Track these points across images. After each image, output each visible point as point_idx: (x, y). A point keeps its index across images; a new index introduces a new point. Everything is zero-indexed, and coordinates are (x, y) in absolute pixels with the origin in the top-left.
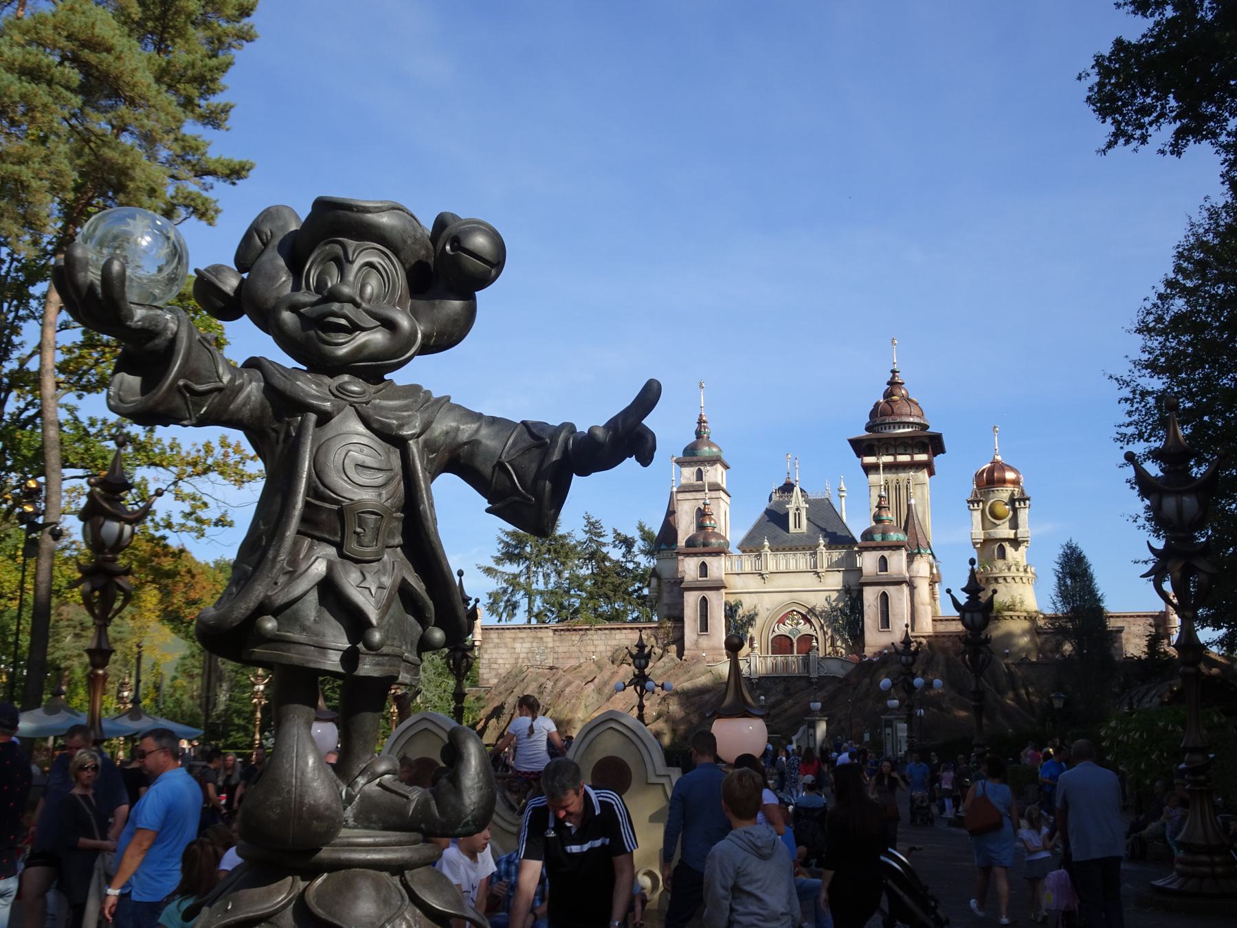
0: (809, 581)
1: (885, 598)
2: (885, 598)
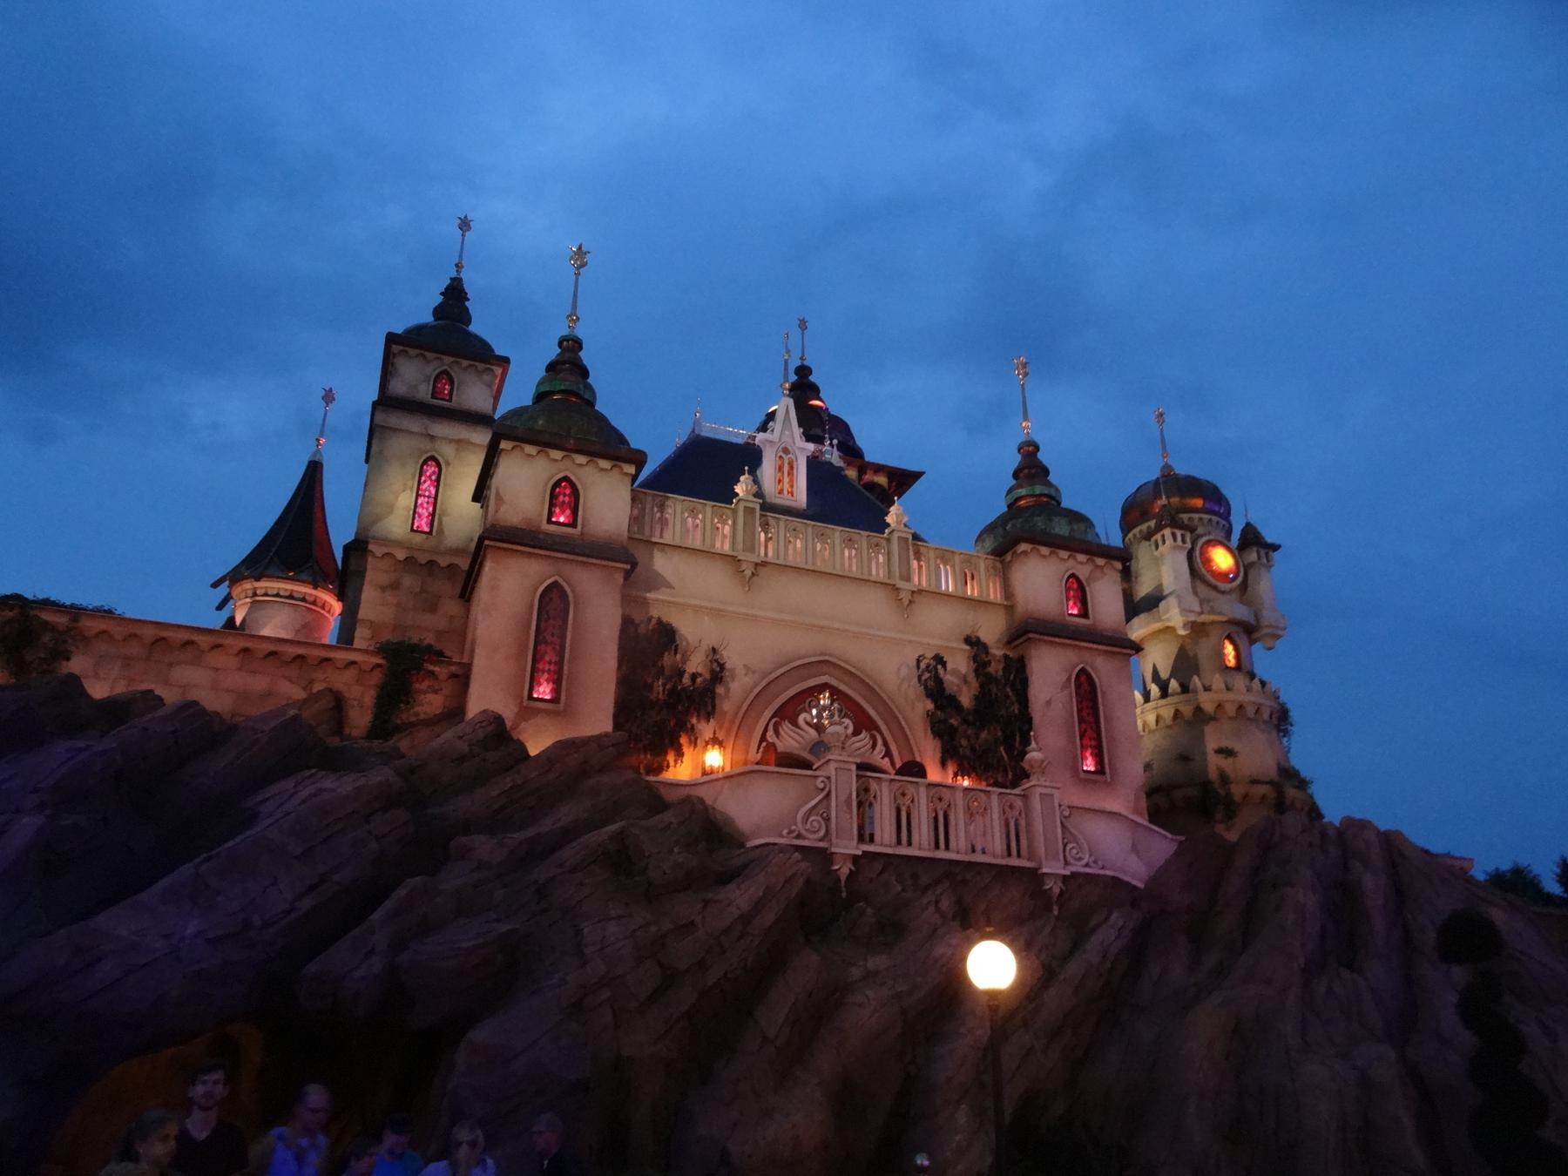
0: (871, 608)
1: (1086, 691)
2: (1086, 691)
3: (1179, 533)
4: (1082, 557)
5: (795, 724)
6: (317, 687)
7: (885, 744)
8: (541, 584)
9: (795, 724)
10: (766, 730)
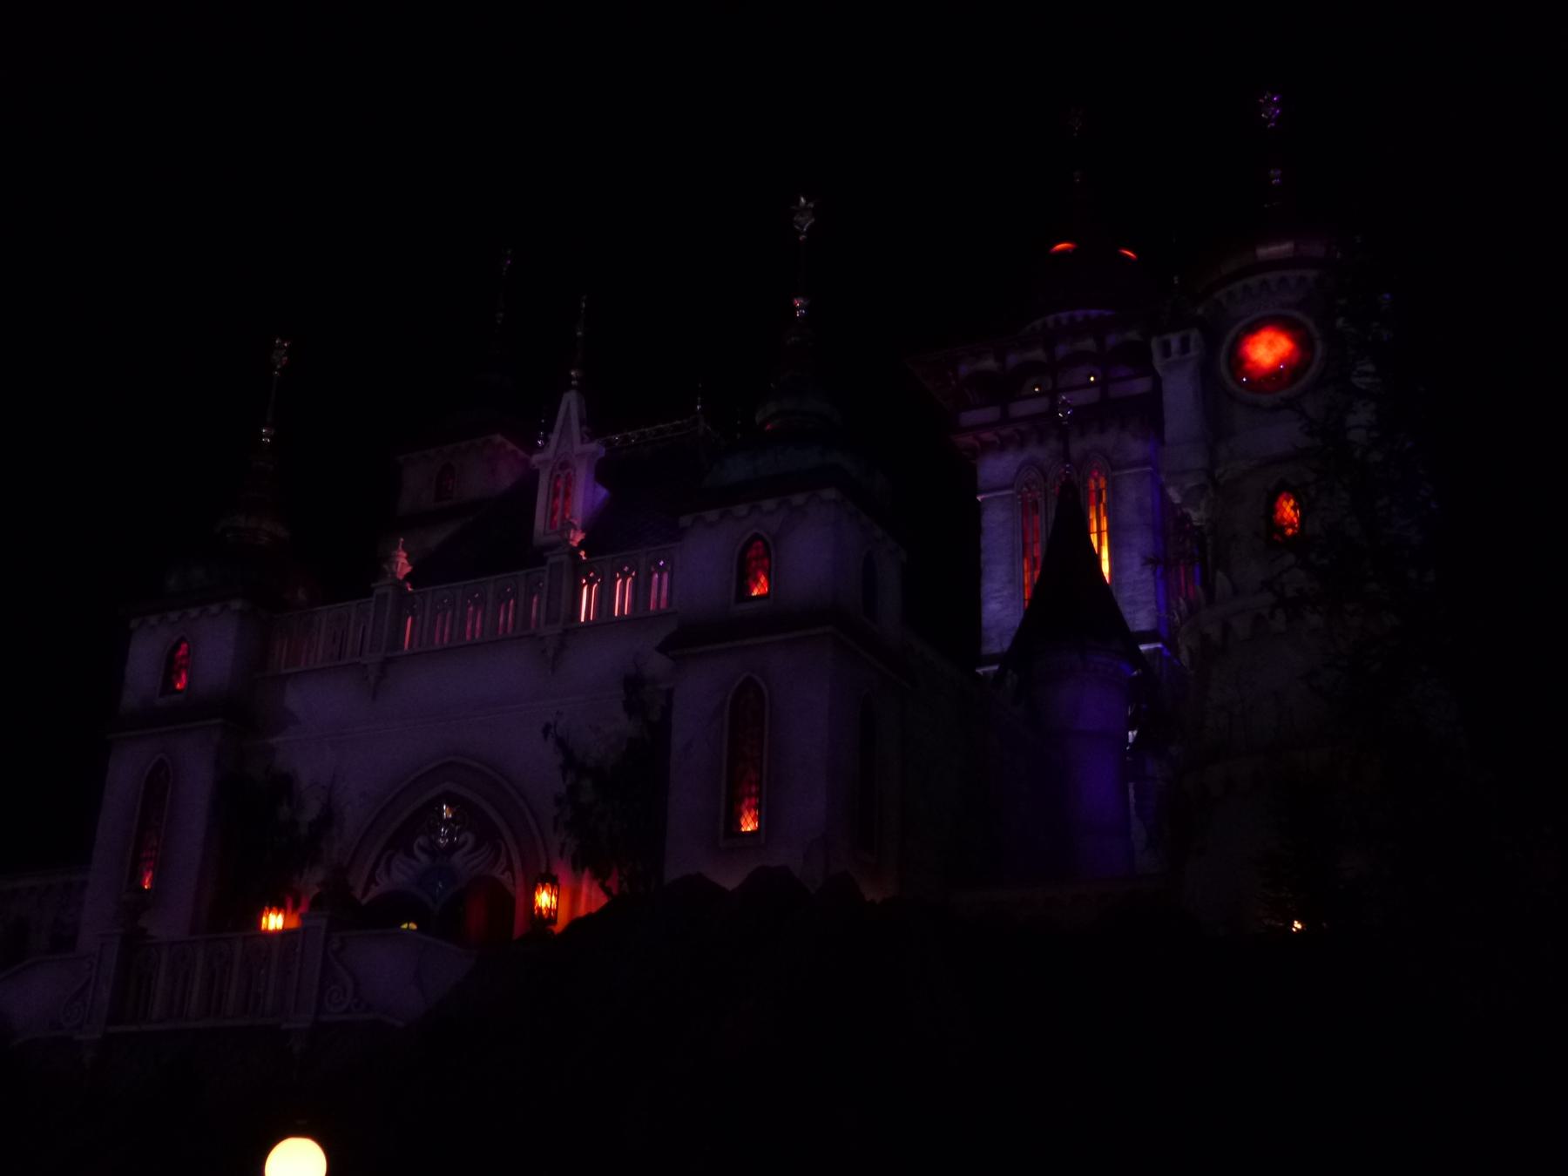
3: (1174, 341)
4: (769, 504)
5: (410, 853)
7: (510, 861)
9: (410, 853)
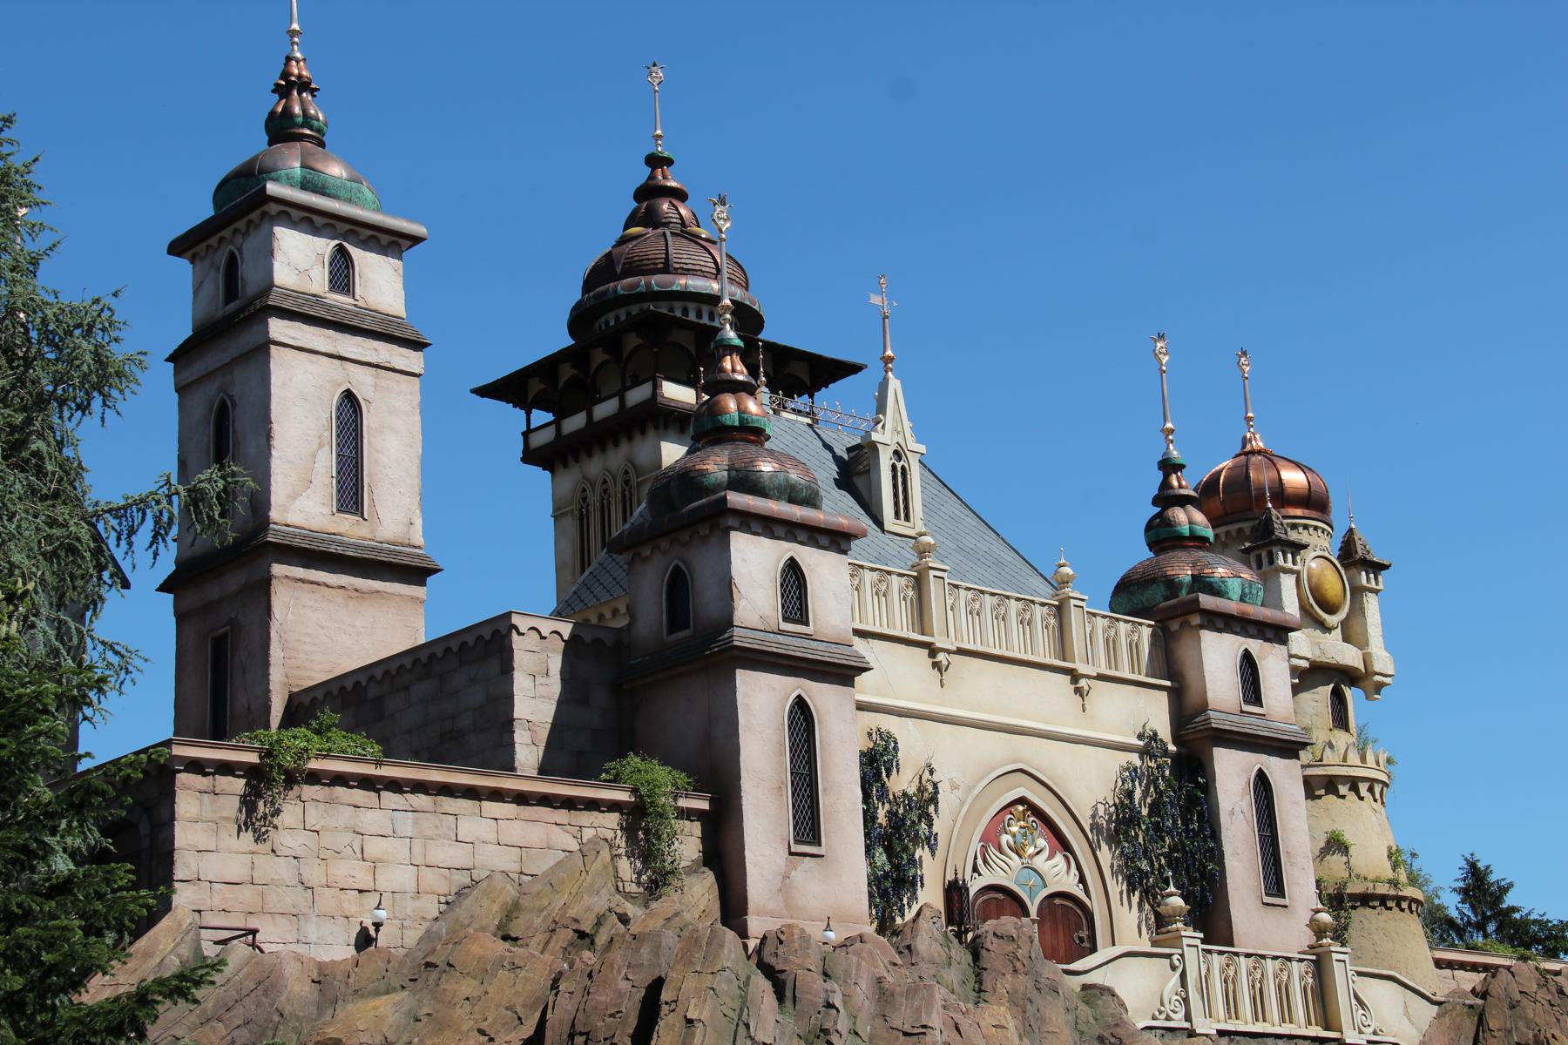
6: (588, 834)
8: (787, 700)
10: (976, 858)
